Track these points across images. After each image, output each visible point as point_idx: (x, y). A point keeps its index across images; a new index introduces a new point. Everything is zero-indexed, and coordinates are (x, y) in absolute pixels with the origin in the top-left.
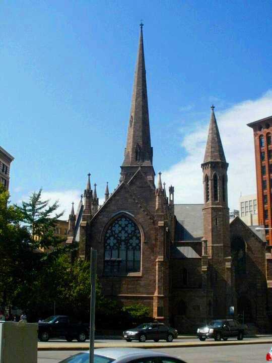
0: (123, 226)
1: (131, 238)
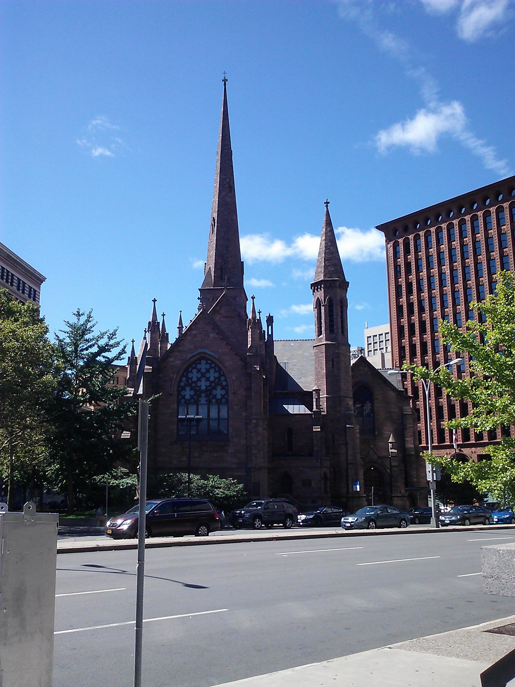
0: (203, 370)
1: (215, 388)
